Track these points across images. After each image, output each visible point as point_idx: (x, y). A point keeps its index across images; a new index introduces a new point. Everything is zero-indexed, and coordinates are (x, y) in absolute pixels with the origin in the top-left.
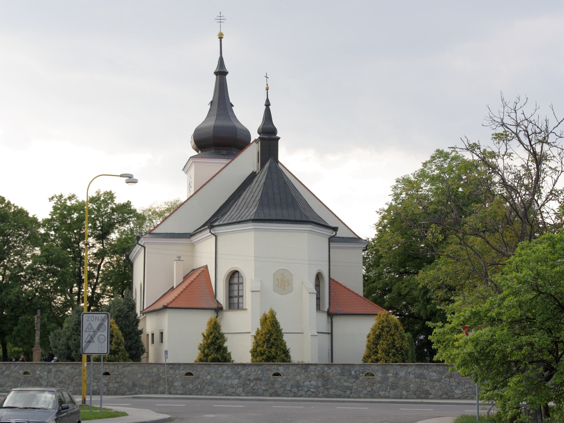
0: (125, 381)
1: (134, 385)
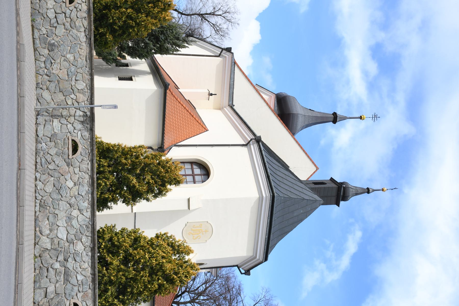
0: (60, 31)
1: (51, 47)
